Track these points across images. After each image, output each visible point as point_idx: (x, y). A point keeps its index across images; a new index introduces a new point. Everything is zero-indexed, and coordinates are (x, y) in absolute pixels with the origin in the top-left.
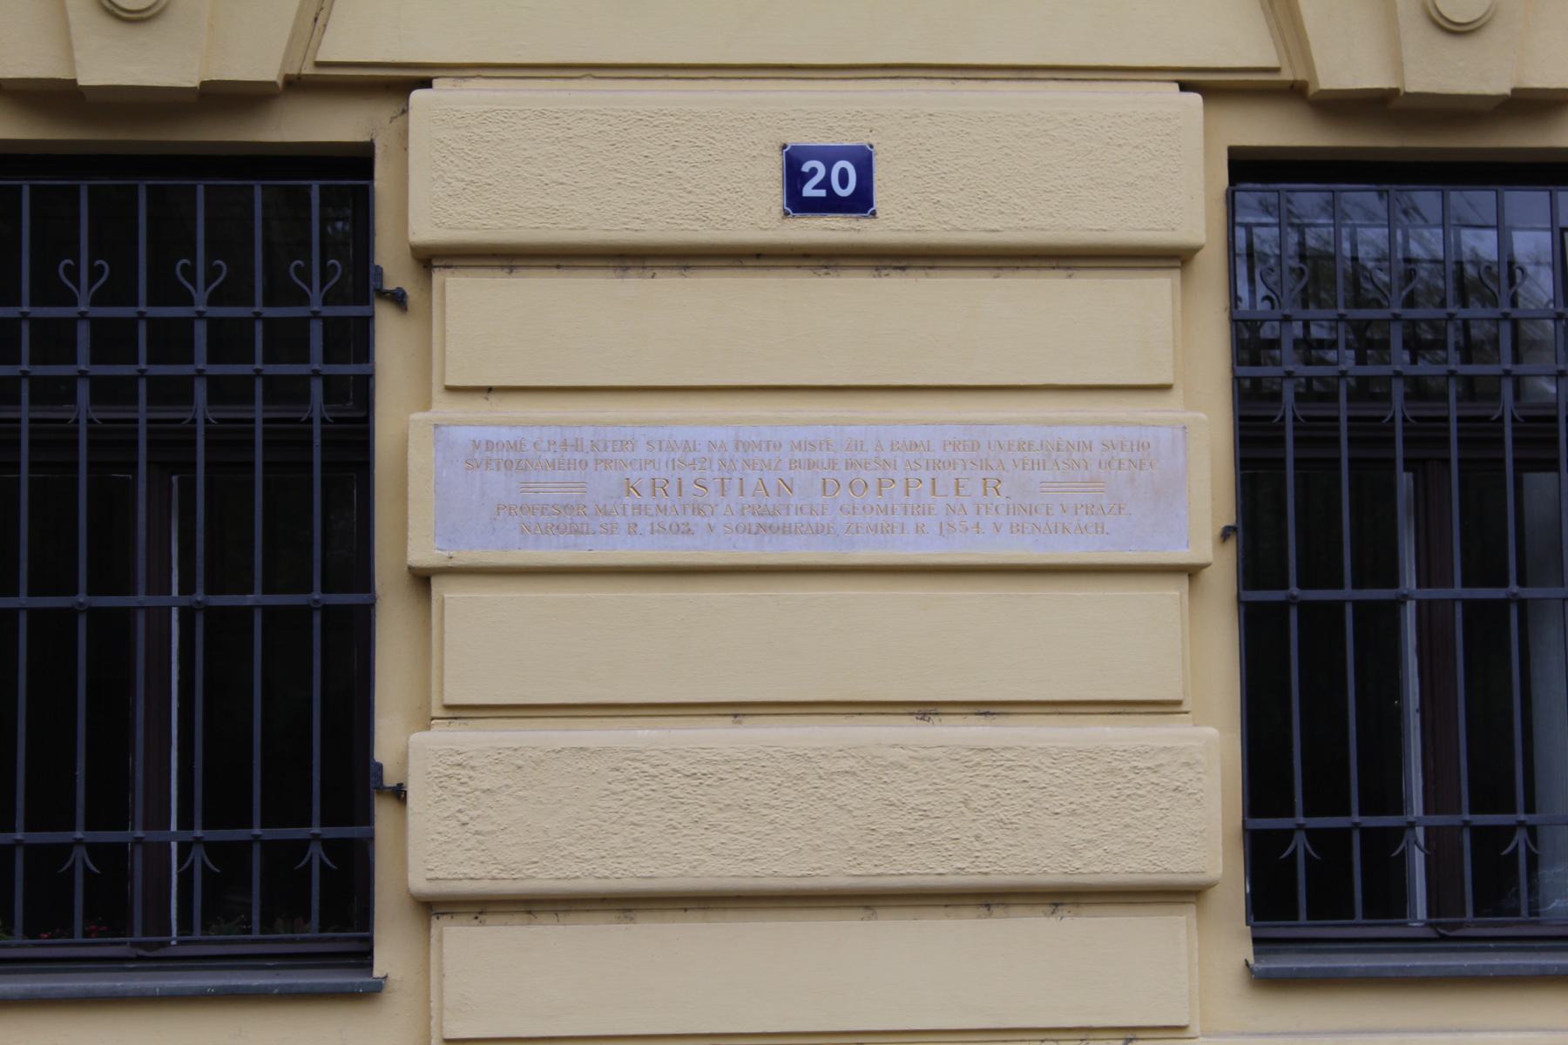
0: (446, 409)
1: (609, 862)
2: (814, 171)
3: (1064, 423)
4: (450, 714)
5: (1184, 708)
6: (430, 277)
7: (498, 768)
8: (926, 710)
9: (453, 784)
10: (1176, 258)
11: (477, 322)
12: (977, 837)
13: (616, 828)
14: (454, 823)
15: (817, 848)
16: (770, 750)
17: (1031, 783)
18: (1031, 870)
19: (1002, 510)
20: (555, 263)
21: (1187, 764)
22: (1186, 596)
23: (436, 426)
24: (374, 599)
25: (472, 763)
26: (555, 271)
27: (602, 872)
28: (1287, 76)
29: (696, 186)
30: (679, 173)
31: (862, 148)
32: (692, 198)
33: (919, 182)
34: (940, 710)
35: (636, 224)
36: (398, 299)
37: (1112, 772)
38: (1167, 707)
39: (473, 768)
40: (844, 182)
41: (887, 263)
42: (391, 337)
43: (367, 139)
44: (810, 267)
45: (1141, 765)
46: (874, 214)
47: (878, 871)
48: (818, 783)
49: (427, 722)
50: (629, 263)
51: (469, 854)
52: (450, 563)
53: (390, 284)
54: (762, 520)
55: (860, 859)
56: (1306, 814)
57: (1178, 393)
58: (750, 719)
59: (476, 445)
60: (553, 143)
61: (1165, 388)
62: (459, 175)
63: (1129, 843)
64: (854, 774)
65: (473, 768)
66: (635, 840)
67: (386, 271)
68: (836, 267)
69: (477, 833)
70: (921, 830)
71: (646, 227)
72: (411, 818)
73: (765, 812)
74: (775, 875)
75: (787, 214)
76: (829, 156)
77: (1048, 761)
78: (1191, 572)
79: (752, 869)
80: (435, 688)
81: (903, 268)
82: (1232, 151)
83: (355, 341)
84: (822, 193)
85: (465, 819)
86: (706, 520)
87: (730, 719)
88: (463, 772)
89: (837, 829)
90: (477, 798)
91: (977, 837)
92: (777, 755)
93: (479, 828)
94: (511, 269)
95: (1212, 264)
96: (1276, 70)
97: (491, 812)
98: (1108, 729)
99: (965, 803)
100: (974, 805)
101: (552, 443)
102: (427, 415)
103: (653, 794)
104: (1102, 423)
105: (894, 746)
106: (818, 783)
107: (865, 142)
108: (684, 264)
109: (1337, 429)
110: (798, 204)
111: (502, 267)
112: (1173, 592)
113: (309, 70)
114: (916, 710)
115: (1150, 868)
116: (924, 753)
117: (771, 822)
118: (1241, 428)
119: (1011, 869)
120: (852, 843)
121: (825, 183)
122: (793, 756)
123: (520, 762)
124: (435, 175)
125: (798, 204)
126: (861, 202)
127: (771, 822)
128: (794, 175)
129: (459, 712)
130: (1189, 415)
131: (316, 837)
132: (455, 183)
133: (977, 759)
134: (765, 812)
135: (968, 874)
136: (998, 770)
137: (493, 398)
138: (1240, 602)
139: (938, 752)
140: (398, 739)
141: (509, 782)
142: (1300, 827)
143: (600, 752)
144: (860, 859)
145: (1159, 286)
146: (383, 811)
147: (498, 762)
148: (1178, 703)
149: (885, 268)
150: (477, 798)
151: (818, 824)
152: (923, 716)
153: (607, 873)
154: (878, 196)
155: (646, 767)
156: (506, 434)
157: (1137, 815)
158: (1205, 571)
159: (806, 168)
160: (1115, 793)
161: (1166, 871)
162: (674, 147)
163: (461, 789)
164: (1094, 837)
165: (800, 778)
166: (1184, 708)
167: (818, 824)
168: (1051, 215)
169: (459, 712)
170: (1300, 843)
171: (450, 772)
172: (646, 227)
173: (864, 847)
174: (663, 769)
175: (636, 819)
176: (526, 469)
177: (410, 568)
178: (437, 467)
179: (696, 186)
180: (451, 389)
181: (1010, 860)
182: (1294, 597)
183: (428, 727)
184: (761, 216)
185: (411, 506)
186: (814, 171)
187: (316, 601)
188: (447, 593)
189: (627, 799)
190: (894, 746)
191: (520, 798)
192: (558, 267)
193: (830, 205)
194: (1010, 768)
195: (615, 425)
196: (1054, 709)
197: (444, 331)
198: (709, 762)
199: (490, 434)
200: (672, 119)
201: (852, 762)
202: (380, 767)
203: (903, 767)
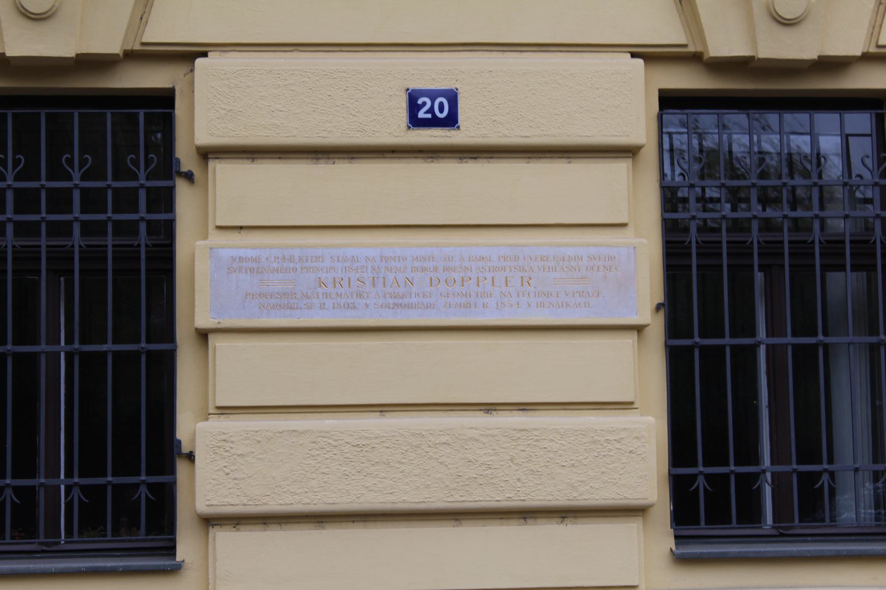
0: (217, 239)
2: (424, 104)
3: (567, 245)
5: (635, 406)
6: (207, 164)
8: (489, 408)
10: (630, 152)
12: (519, 480)
13: (314, 475)
14: (222, 474)
15: (428, 487)
16: (401, 431)
17: (549, 449)
18: (550, 498)
21: (637, 438)
23: (211, 248)
24: (176, 346)
25: (232, 439)
26: (278, 160)
27: (306, 500)
28: (691, 49)
29: (358, 112)
30: (348, 105)
31: (452, 90)
33: (484, 109)
35: (324, 134)
36: (189, 177)
37: (594, 442)
39: (232, 442)
40: (441, 110)
41: (466, 155)
42: (185, 198)
43: (171, 86)
44: (422, 158)
45: (611, 438)
46: (458, 127)
47: (463, 499)
48: (428, 449)
50: (320, 156)
51: (230, 491)
52: (219, 326)
53: (184, 168)
54: (396, 301)
55: (453, 493)
56: (705, 465)
60: (276, 88)
61: (623, 225)
62: (223, 106)
63: (605, 483)
64: (449, 444)
65: (232, 442)
66: (325, 482)
68: (437, 158)
69: (235, 479)
73: (399, 466)
74: (404, 502)
75: (409, 128)
76: (433, 95)
78: (639, 329)
80: (210, 397)
81: (475, 158)
82: (661, 91)
83: (165, 201)
84: (429, 116)
85: (228, 471)
86: (364, 301)
87: (378, 414)
89: (439, 475)
91: (519, 480)
92: (405, 434)
93: (236, 476)
94: (253, 159)
95: (650, 155)
96: (685, 46)
98: (592, 418)
99: (512, 460)
101: (276, 258)
102: (206, 242)
106: (428, 449)
107: (453, 87)
109: (721, 248)
110: (415, 122)
111: (248, 158)
112: (628, 341)
113: (137, 47)
114: (483, 408)
115: (617, 497)
116: (489, 432)
117: (402, 472)
120: (447, 483)
121: (431, 110)
122: (414, 435)
123: (259, 439)
125: (415, 122)
126: (451, 121)
127: (402, 472)
128: (413, 106)
129: (224, 410)
133: (518, 435)
134: (399, 466)
135: (513, 500)
136: (530, 442)
137: (243, 232)
138: (666, 346)
139: (496, 432)
140: (190, 426)
141: (253, 450)
143: (303, 433)
144: (453, 493)
146: (181, 467)
147: (247, 439)
148: (632, 403)
149: (465, 158)
152: (488, 411)
153: (309, 501)
155: (331, 441)
156: (250, 253)
157: (609, 466)
159: (420, 102)
163: (226, 454)
164: (585, 479)
165: (418, 446)
166: (635, 406)
168: (559, 128)
169: (224, 410)
171: (219, 444)
174: (340, 442)
175: (325, 470)
177: (196, 329)
179: (358, 112)
180: (219, 228)
182: (697, 343)
183: (207, 419)
184: (395, 129)
185: (196, 293)
186: (424, 104)
189: (320, 459)
191: (259, 459)
192: (280, 158)
193: (434, 122)
194: (537, 441)
196: (562, 407)
198: (367, 438)
199: (242, 253)
200: (344, 74)
202: (180, 442)
203: (477, 440)
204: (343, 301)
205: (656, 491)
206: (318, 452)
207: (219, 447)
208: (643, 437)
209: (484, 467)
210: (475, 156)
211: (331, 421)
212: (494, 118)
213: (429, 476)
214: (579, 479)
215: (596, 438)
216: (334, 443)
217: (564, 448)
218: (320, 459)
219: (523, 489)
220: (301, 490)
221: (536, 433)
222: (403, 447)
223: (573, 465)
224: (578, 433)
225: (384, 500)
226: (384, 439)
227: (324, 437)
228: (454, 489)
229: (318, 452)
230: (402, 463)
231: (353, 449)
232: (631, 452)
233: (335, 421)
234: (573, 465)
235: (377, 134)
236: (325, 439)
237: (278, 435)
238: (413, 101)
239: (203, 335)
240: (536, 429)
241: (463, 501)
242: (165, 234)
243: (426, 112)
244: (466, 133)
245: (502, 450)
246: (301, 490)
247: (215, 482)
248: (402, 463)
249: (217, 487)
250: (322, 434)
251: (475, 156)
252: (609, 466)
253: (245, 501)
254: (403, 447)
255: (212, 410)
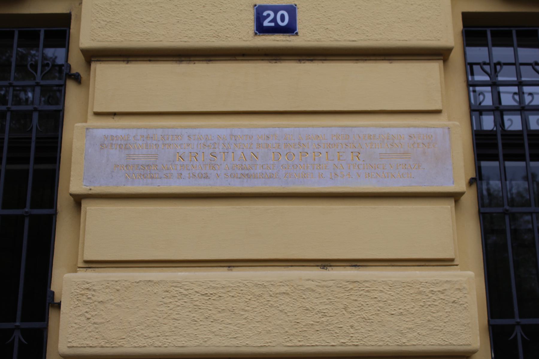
0: (93, 122)
1: (161, 338)
2: (269, 15)
3: (390, 126)
4: (87, 266)
5: (455, 263)
6: (90, 65)
7: (107, 290)
8: (325, 263)
9: (84, 298)
10: (440, 54)
11: (110, 84)
12: (352, 327)
13: (166, 321)
14: (83, 318)
15: (269, 332)
16: (245, 282)
18: (380, 343)
19: (361, 167)
20: (148, 59)
21: (459, 289)
22: (454, 209)
23: (87, 129)
24: (56, 213)
25: (94, 288)
26: (149, 62)
27: (158, 343)
30: (206, 17)
31: (292, 6)
32: (212, 27)
34: (332, 264)
35: (186, 39)
36: (77, 79)
37: (420, 293)
38: (446, 262)
39: (94, 290)
40: (283, 18)
41: (304, 58)
42: (72, 92)
43: (68, 12)
44: (268, 60)
45: (435, 290)
46: (297, 34)
47: (301, 344)
48: (269, 298)
49: (75, 269)
50: (183, 59)
51: (90, 334)
52: (90, 192)
53: (74, 70)
54: (243, 172)
55: (291, 338)
56: (521, 317)
57: (444, 115)
58: (236, 268)
59: (106, 137)
62: (104, 19)
63: (431, 330)
64: (288, 294)
65: (94, 290)
66: (175, 327)
67: (72, 66)
69: (95, 323)
70: (322, 323)
71: (190, 40)
72: (61, 316)
73: (242, 313)
74: (247, 346)
75: (256, 34)
76: (276, 9)
77: (387, 288)
78: (456, 197)
79: (235, 342)
80: (80, 253)
81: (312, 60)
82: (467, 17)
83: (55, 97)
84: (273, 24)
85: (89, 316)
86: (216, 172)
87: (226, 268)
88: (89, 292)
89: (279, 322)
90: (96, 306)
91: (352, 327)
92: (249, 284)
93: (96, 321)
94: (128, 62)
97: (102, 313)
98: (417, 272)
99: (345, 309)
100: (350, 310)
101: (142, 136)
102: (84, 124)
103: (185, 304)
104: (409, 127)
105: (308, 280)
106: (269, 298)
107: (293, 4)
108: (209, 59)
110: (261, 30)
111: (124, 61)
112: (448, 206)
114: (320, 264)
115: (442, 343)
116: (324, 283)
117: (245, 319)
118: (476, 139)
119: (370, 343)
120: (287, 329)
121: (274, 20)
122: (256, 285)
123: (118, 288)
124: (93, 19)
125: (261, 30)
126: (290, 29)
127: (245, 319)
128: (259, 19)
129: (91, 264)
130: (451, 123)
131: (17, 327)
132: (102, 22)
133: (351, 286)
134: (242, 313)
135: (347, 345)
136: (361, 292)
137: (116, 118)
139: (331, 283)
140: (66, 281)
141: (112, 297)
142: (518, 323)
143: (158, 283)
144: (291, 338)
145: (434, 67)
146: (52, 314)
148: (452, 260)
149: (303, 60)
150: (96, 306)
151: (269, 320)
152: (324, 267)
153: (160, 344)
154: (300, 27)
155: (182, 290)
156: (120, 132)
157: (434, 315)
158: (476, 354)
159: (265, 14)
160: (422, 304)
161: (451, 344)
162: (204, 6)
163: (88, 301)
164: (412, 326)
166: (455, 263)
167: (269, 320)
168: (381, 34)
169: (91, 264)
170: (518, 331)
171: (83, 292)
172: (190, 40)
173: (293, 331)
174: (190, 291)
175: (176, 317)
176: (129, 149)
177: (71, 195)
178: (89, 152)
179: (214, 23)
180: (97, 114)
181: (368, 338)
182: (507, 210)
184: (245, 36)
185: (73, 165)
186: (269, 15)
187: (26, 212)
188: (90, 209)
189: (172, 306)
190: (308, 280)
191: (117, 306)
192: (150, 61)
193: (276, 30)
194: (368, 291)
195: (172, 128)
196: (389, 264)
197: (94, 88)
198: (214, 288)
199: (113, 132)
201: (287, 288)
203: (313, 291)
204: (198, 172)
205: (479, 338)
206: (171, 300)
207: (83, 295)
208: (464, 288)
209: (320, 315)
210: (312, 58)
211: (183, 273)
212: (326, 27)
213: (270, 322)
214: (407, 326)
215: (422, 289)
216: (185, 292)
217: (392, 298)
218: (172, 306)
219: (356, 335)
220: (154, 334)
221: (367, 284)
222: (247, 296)
223: (401, 314)
224: (405, 284)
225: (229, 344)
226: (230, 289)
227: (176, 287)
228: (293, 335)
229: (171, 300)
230: (246, 311)
231: (201, 297)
232: (454, 302)
233: (187, 274)
234: (401, 314)
235: (229, 39)
236: (177, 289)
237: (135, 284)
238: (260, 13)
239: (78, 200)
240: (367, 281)
241: (301, 346)
242: (54, 120)
243: (270, 22)
244: (306, 37)
245: (336, 300)
246: (154, 334)
247: (77, 326)
248: (246, 311)
249: (78, 330)
250: (174, 284)
251: (312, 58)
252: (434, 315)
253: (103, 344)
254: (247, 296)
255: (80, 264)
